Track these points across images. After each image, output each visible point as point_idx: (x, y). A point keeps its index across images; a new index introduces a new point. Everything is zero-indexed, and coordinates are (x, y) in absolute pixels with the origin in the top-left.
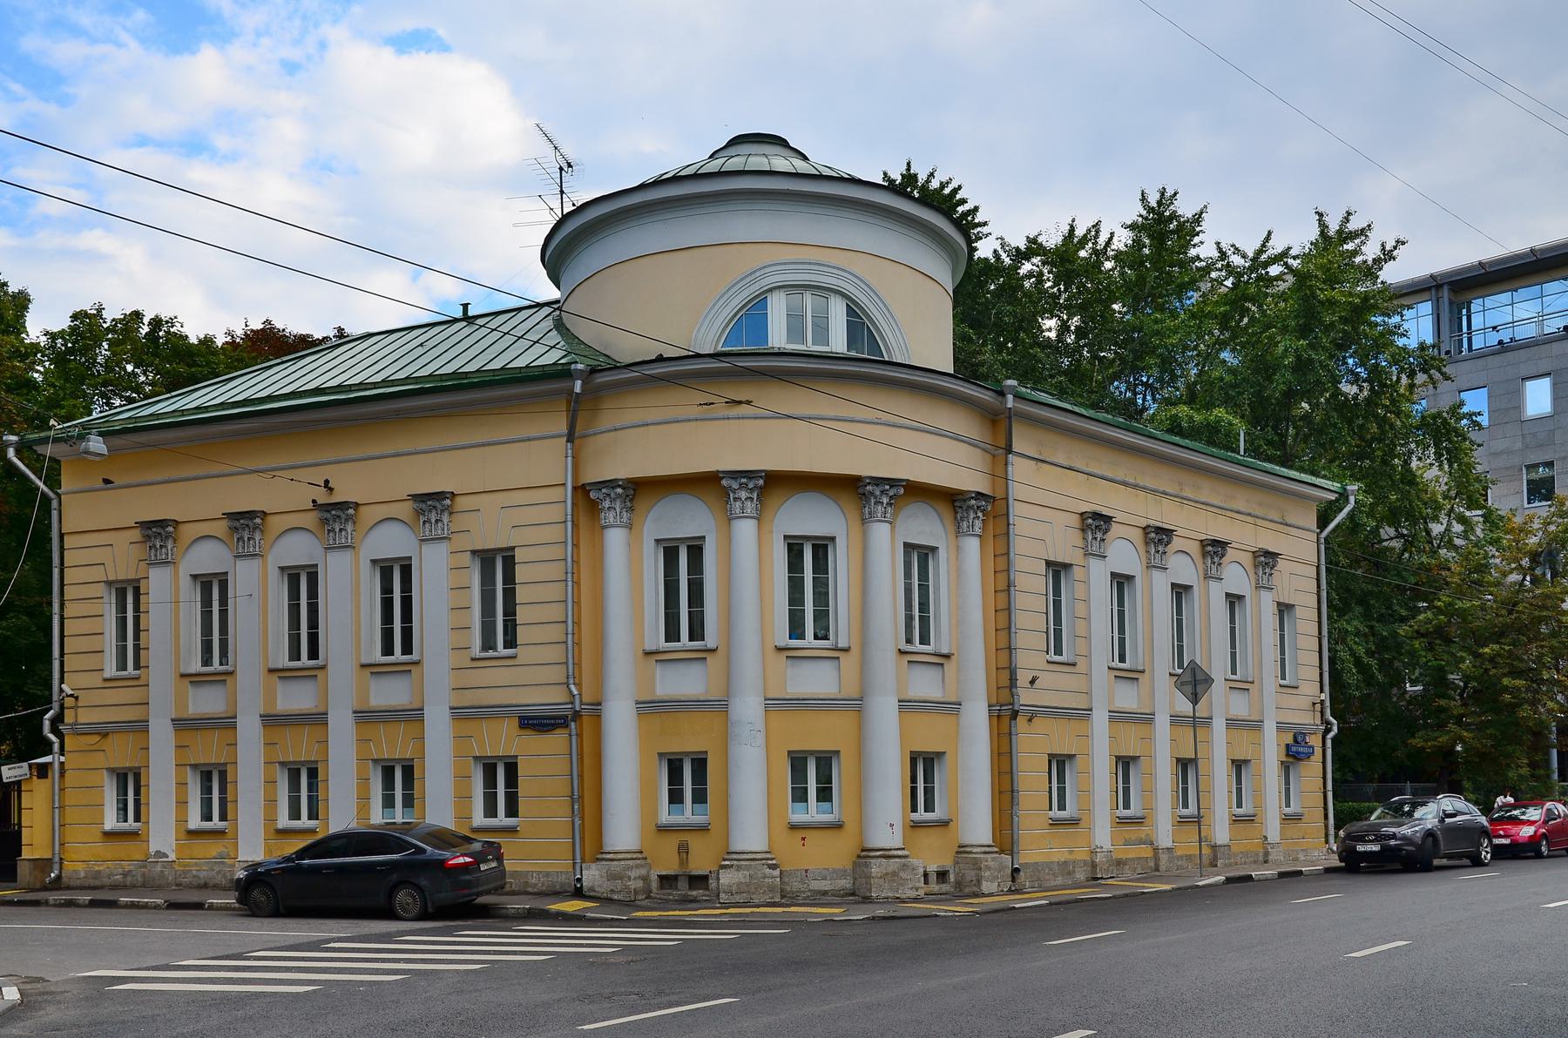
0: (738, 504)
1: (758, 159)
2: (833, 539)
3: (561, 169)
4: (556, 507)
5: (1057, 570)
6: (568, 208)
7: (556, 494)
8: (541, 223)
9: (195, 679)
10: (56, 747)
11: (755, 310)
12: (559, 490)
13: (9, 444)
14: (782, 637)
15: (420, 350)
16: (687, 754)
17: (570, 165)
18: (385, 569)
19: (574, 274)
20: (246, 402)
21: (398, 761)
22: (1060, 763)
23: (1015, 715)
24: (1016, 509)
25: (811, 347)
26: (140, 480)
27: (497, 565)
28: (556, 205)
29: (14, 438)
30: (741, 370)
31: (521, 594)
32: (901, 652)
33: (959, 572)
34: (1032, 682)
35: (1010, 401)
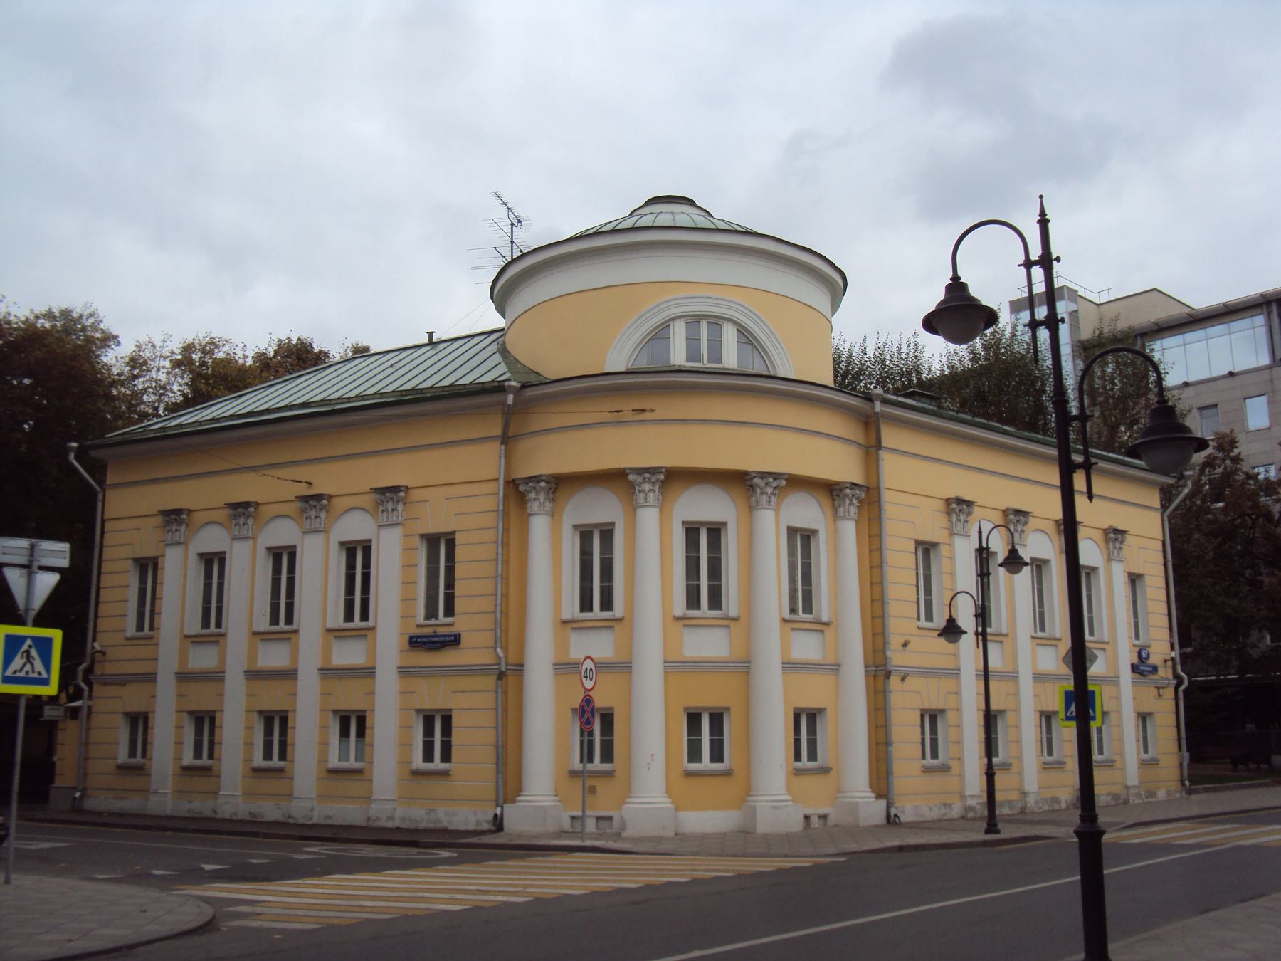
0: (642, 495)
1: (665, 216)
2: (724, 524)
3: (512, 224)
4: (489, 499)
5: (926, 549)
6: (517, 254)
7: (490, 487)
8: (494, 267)
9: (196, 640)
10: (86, 694)
11: (661, 333)
12: (495, 483)
13: (72, 448)
14: (680, 607)
15: (391, 370)
16: (705, 709)
17: (519, 221)
18: (350, 549)
19: (513, 311)
20: (250, 414)
21: (438, 711)
22: (932, 717)
23: (888, 675)
24: (887, 496)
25: (705, 363)
26: (204, 469)
27: (441, 546)
29: (74, 445)
30: (646, 386)
31: (460, 571)
32: (785, 621)
33: (836, 551)
34: (905, 645)
35: (878, 407)
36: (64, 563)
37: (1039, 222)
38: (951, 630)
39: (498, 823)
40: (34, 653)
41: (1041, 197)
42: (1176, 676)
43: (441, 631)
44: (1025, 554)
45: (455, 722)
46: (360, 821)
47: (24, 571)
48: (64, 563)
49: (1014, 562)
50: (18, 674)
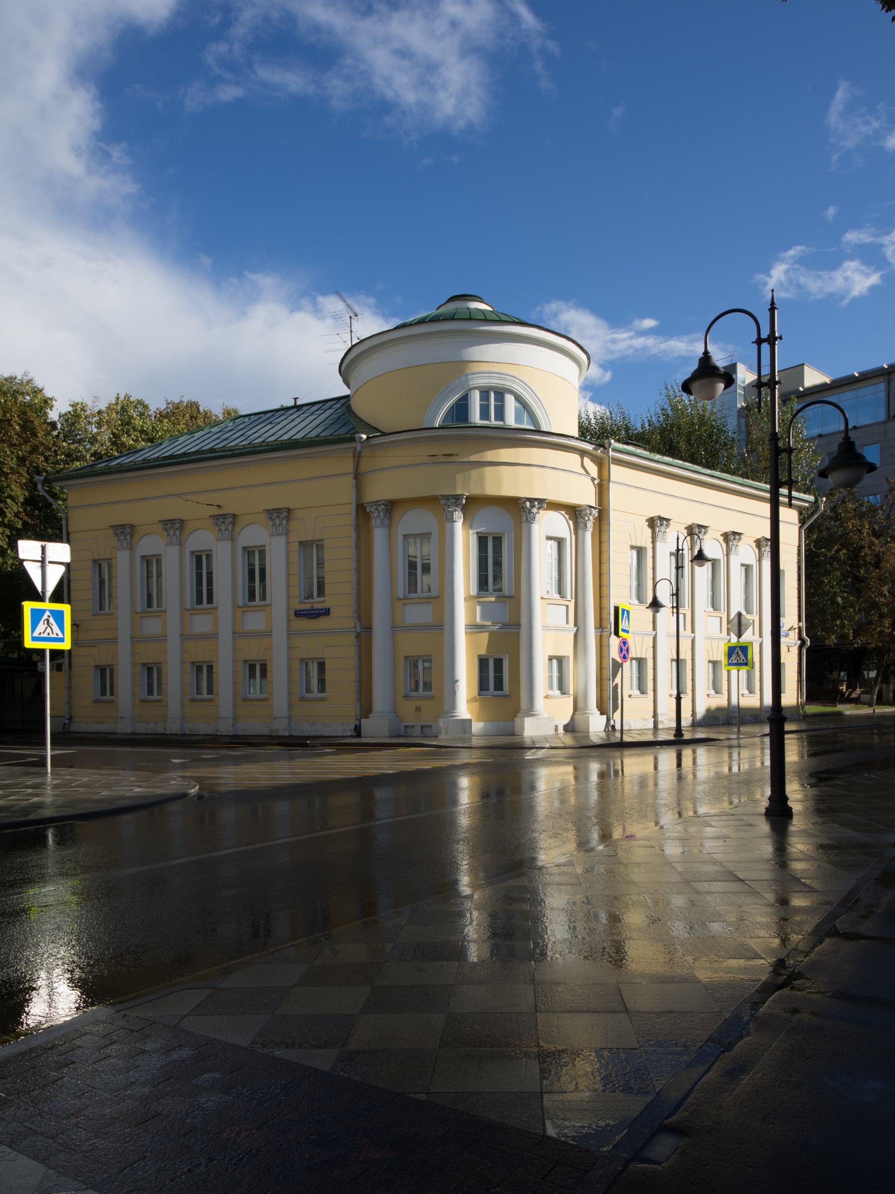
8: (339, 350)
15: (313, 417)
25: (493, 422)
28: (348, 339)
36: (67, 559)
37: (770, 310)
38: (655, 605)
39: (358, 731)
40: (52, 620)
41: (773, 291)
42: (800, 638)
43: (317, 606)
44: (708, 553)
45: (327, 666)
46: (266, 732)
47: (40, 564)
48: (67, 559)
49: (700, 558)
50: (42, 635)
